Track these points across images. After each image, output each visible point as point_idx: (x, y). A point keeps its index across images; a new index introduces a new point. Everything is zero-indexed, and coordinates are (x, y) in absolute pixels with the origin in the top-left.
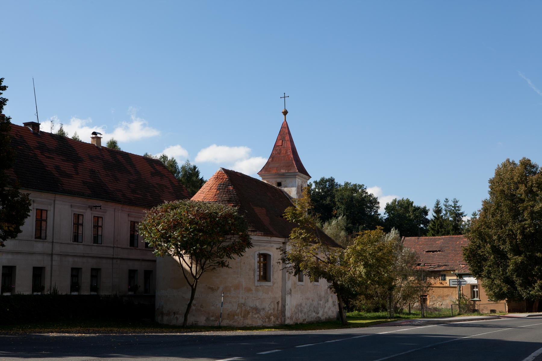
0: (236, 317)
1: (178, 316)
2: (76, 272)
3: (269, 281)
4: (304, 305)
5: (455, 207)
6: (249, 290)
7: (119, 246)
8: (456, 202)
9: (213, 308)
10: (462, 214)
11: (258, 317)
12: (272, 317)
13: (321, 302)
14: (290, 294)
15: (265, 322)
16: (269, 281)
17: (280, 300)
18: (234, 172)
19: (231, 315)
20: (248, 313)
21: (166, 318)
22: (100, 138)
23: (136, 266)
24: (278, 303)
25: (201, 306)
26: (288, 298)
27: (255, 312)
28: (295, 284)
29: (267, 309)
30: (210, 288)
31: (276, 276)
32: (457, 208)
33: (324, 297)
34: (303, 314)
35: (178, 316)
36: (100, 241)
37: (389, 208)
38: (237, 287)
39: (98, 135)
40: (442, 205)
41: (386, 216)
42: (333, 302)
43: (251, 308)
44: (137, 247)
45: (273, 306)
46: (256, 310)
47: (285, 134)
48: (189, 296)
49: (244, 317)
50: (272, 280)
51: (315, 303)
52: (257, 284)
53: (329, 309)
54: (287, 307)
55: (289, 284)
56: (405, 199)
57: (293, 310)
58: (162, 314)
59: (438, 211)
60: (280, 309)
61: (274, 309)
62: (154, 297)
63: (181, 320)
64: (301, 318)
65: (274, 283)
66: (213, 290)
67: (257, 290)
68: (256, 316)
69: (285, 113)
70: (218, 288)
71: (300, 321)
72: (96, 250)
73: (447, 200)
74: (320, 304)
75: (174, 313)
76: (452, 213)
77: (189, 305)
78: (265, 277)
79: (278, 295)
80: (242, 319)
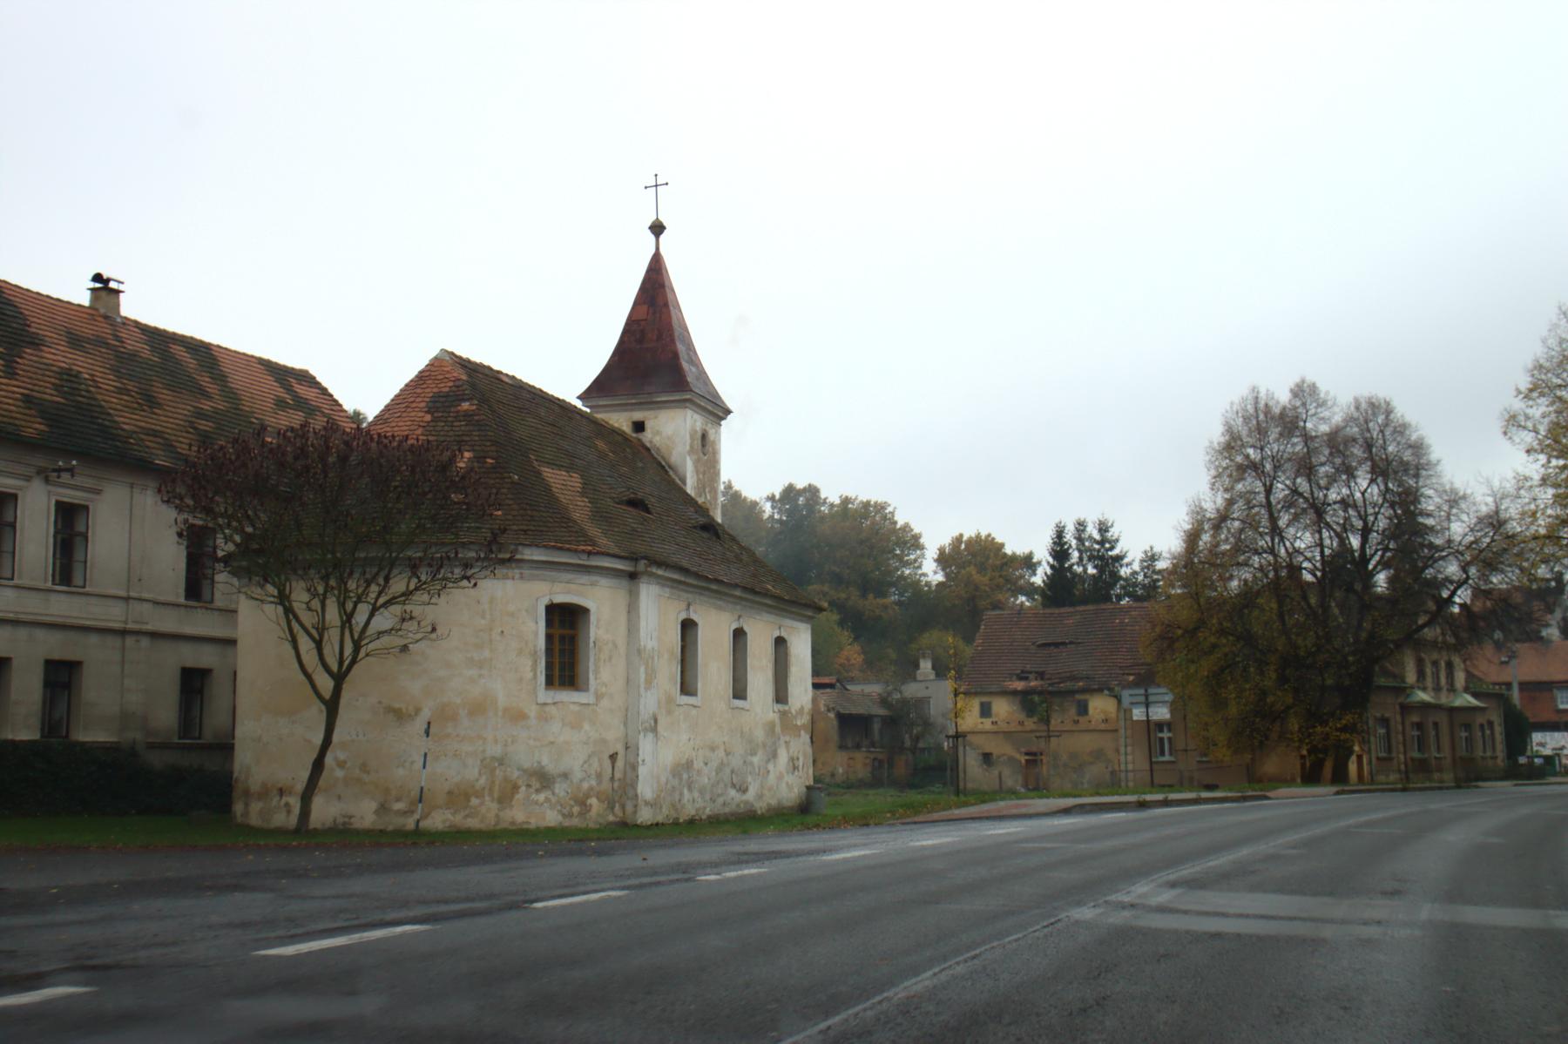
0: (474, 801)
4: (698, 764)
5: (1102, 543)
6: (518, 716)
7: (145, 595)
8: (1103, 528)
9: (401, 772)
11: (547, 800)
12: (593, 801)
13: (756, 760)
14: (654, 730)
15: (571, 815)
17: (620, 748)
18: (490, 368)
19: (459, 797)
20: (515, 788)
21: (256, 807)
22: (118, 292)
24: (613, 757)
25: (364, 768)
26: (646, 745)
27: (536, 784)
28: (670, 700)
29: (578, 775)
31: (605, 674)
33: (764, 746)
34: (696, 794)
36: (78, 580)
38: (479, 708)
39: (112, 285)
40: (1070, 537)
41: (940, 577)
42: (792, 760)
43: (525, 771)
44: (212, 601)
45: (596, 765)
46: (544, 779)
47: (655, 291)
49: (500, 801)
50: (592, 689)
51: (736, 762)
52: (544, 695)
53: (780, 778)
54: (642, 771)
55: (649, 703)
56: (983, 534)
57: (663, 779)
58: (247, 793)
59: (1060, 552)
60: (618, 775)
61: (599, 776)
64: (693, 804)
65: (599, 697)
67: (544, 718)
68: (541, 797)
69: (657, 229)
70: (418, 711)
71: (689, 811)
72: (63, 607)
73: (1081, 526)
74: (751, 764)
75: (281, 792)
77: (318, 765)
80: (494, 806)
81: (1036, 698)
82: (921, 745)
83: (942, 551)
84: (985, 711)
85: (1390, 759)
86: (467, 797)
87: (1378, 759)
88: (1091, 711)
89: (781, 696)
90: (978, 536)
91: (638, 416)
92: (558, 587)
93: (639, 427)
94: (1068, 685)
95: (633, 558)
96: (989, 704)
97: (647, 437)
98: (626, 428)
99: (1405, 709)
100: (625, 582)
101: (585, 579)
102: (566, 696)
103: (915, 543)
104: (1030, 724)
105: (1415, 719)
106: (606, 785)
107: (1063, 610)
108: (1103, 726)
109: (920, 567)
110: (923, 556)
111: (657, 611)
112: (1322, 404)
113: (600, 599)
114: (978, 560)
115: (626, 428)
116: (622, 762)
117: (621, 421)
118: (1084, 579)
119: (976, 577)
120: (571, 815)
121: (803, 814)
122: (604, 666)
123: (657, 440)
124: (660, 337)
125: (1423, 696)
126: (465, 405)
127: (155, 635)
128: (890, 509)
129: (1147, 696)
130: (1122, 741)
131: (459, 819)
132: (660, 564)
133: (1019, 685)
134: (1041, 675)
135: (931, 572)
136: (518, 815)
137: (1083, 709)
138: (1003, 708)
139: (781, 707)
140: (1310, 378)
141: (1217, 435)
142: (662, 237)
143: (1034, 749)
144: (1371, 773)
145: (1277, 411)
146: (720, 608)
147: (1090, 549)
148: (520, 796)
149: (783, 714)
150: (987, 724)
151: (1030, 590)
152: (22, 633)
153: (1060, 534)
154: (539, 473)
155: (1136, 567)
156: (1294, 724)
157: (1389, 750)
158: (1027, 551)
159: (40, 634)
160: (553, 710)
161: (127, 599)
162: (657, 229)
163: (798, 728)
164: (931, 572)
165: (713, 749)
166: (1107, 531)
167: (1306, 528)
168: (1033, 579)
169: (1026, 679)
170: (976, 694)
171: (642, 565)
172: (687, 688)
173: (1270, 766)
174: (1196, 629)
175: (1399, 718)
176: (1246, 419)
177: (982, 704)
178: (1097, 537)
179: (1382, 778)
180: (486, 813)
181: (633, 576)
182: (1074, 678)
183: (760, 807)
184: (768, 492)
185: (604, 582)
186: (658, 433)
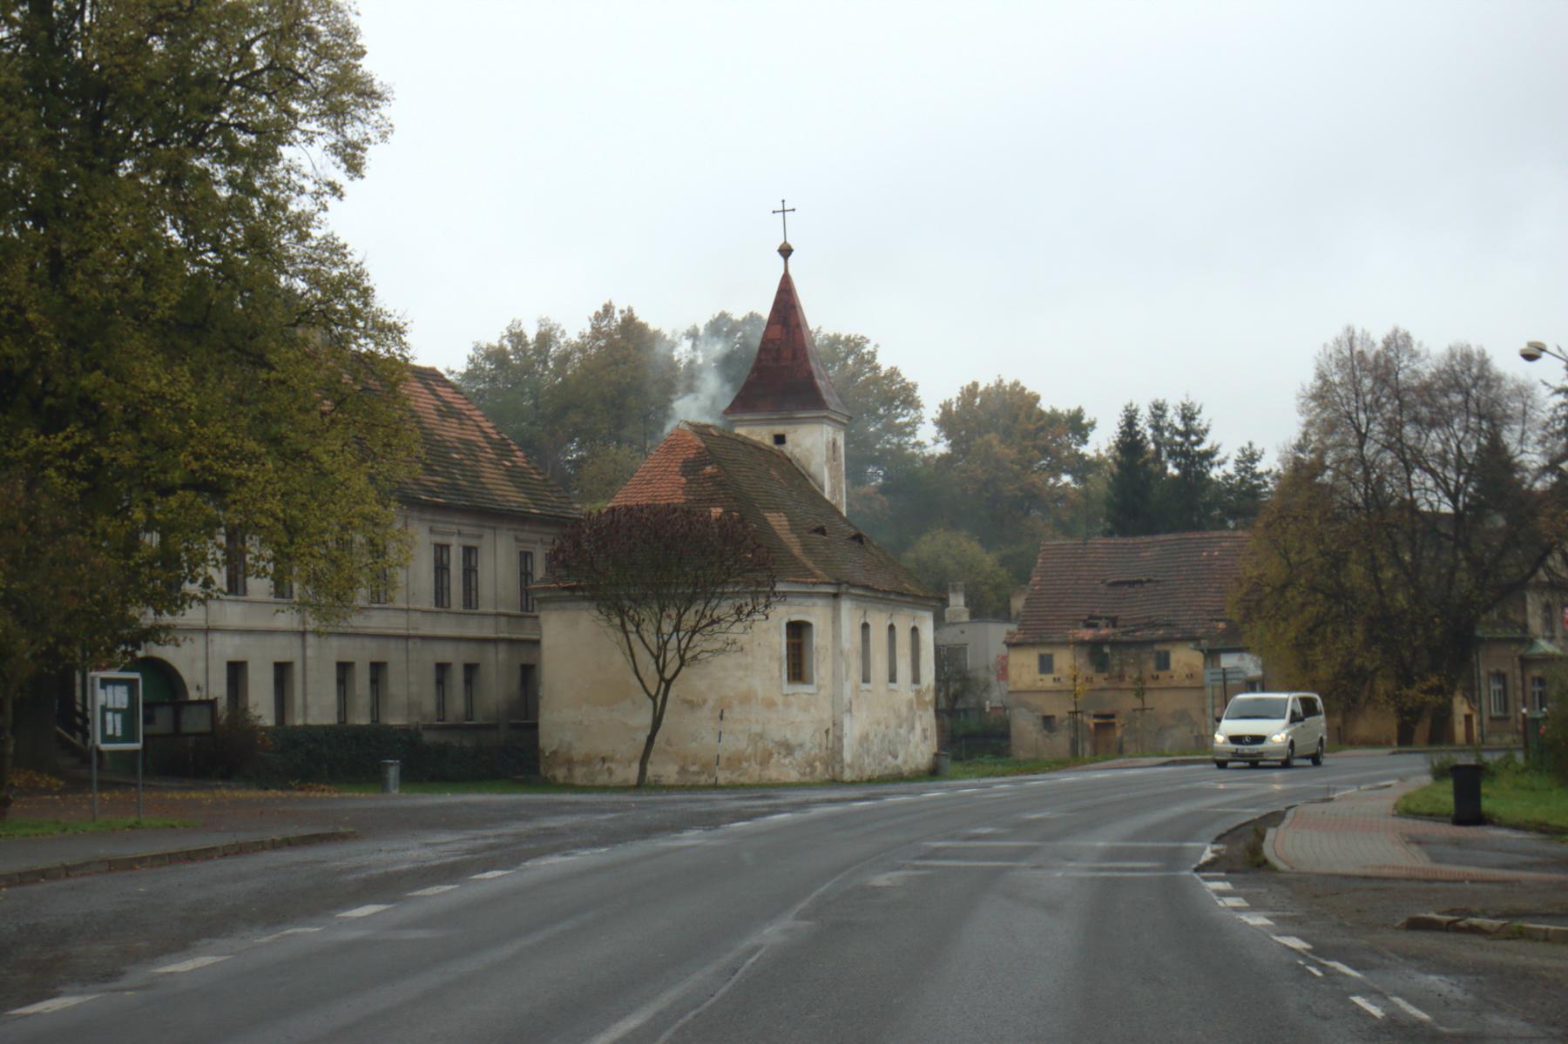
0: (745, 764)
1: (613, 766)
2: (236, 671)
3: (809, 682)
4: (871, 737)
5: (1186, 434)
6: (770, 704)
8: (1188, 415)
10: (1210, 454)
12: (817, 764)
14: (850, 711)
16: (809, 682)
19: (735, 761)
20: (771, 755)
23: (446, 653)
24: (827, 732)
26: (847, 721)
28: (857, 687)
29: (808, 745)
30: (685, 701)
32: (1193, 438)
35: (613, 766)
37: (948, 422)
38: (746, 699)
40: (1144, 426)
41: (942, 448)
42: (924, 730)
46: (788, 748)
48: (645, 718)
52: (788, 688)
54: (846, 741)
56: (1007, 382)
58: (570, 763)
62: (535, 726)
63: (632, 774)
65: (819, 688)
66: (692, 705)
67: (787, 705)
68: (787, 761)
69: (786, 251)
70: (705, 701)
71: (867, 773)
72: (473, 629)
73: (1159, 410)
75: (604, 760)
76: (1177, 453)
77: (651, 740)
78: (798, 668)
79: (827, 715)
80: (758, 767)
81: (1107, 650)
82: (960, 705)
83: (945, 408)
84: (1046, 665)
85: (1506, 719)
86: (740, 761)
87: (1491, 719)
88: (1173, 665)
89: (916, 679)
90: (999, 384)
91: (779, 429)
92: (793, 609)
93: (780, 439)
94: (1146, 634)
95: (838, 584)
96: (1050, 657)
97: (788, 448)
98: (768, 441)
99: (1525, 662)
100: (831, 601)
101: (809, 602)
102: (800, 688)
103: (907, 397)
104: (1100, 680)
105: (1537, 672)
106: (824, 753)
107: (1138, 540)
108: (1187, 683)
109: (913, 433)
110: (920, 419)
111: (849, 614)
112: (1414, 356)
113: (816, 614)
114: (1005, 424)
115: (768, 441)
116: (834, 732)
117: (760, 434)
118: (1158, 483)
119: (999, 449)
120: (804, 774)
121: (933, 772)
122: (821, 667)
123: (797, 452)
124: (794, 357)
125: (1544, 646)
126: (709, 469)
127: (423, 638)
128: (869, 348)
129: (1225, 681)
130: (1209, 701)
131: (735, 777)
132: (853, 586)
133: (1087, 634)
134: (1113, 622)
135: (930, 440)
136: (773, 774)
137: (1164, 662)
138: (1064, 660)
139: (915, 687)
140: (1404, 327)
141: (1308, 379)
142: (790, 259)
143: (1107, 711)
144: (1481, 735)
145: (1370, 355)
146: (881, 611)
147: (1171, 443)
148: (773, 761)
149: (918, 692)
150: (1048, 681)
151: (1082, 468)
152: (358, 642)
153: (1130, 419)
154: (765, 519)
155: (1230, 468)
156: (1382, 686)
157: (1506, 708)
158: (1074, 408)
159: (367, 642)
160: (792, 699)
161: (408, 610)
162: (786, 251)
163: (926, 703)
164: (930, 440)
165: (879, 724)
166: (1192, 418)
167: (1392, 498)
168: (1083, 449)
169: (1094, 626)
170: (1033, 645)
171: (843, 588)
172: (866, 680)
173: (1362, 728)
174: (1284, 587)
175: (1518, 672)
176: (1341, 365)
177: (1042, 657)
178: (1181, 427)
179: (1495, 740)
180: (753, 773)
181: (836, 596)
182: (1153, 625)
183: (906, 769)
184: (686, 326)
185: (820, 602)
186: (798, 445)
